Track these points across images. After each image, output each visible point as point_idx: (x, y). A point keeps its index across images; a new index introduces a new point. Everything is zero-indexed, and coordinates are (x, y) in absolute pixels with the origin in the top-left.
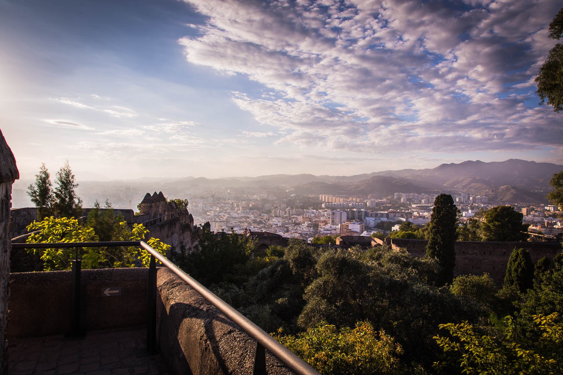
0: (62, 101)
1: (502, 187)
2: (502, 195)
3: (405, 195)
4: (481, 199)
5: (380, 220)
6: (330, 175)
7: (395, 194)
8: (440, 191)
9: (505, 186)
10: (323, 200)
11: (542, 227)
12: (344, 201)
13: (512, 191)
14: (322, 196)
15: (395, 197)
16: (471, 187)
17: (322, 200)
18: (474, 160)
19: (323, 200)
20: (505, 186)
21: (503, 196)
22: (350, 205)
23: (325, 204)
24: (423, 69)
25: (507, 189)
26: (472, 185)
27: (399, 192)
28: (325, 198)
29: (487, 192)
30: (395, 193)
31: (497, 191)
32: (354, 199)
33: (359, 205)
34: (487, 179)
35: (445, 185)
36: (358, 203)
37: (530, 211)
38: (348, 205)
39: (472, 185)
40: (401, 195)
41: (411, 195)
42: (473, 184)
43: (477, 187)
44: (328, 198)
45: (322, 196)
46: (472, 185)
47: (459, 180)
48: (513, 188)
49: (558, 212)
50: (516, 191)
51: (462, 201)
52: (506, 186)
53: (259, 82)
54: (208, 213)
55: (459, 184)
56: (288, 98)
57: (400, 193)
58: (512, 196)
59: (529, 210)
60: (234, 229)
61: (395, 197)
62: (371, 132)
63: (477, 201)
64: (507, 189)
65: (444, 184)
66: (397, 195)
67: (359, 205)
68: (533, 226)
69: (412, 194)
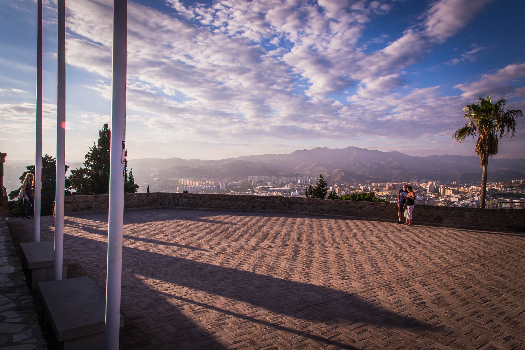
0: (93, 88)
6: (201, 159)
10: (182, 184)
12: (199, 184)
13: (342, 174)
14: (181, 180)
16: (316, 170)
17: (181, 183)
18: (322, 147)
19: (182, 184)
22: (203, 187)
23: (179, 188)
24: (190, 14)
27: (252, 175)
28: (181, 181)
32: (210, 182)
33: (211, 187)
36: (213, 185)
37: (341, 191)
38: (202, 188)
40: (255, 178)
44: (186, 181)
45: (181, 180)
54: (350, 186)
57: (254, 176)
58: (341, 177)
59: (340, 190)
61: (249, 180)
62: (384, 136)
64: (339, 172)
67: (211, 187)
69: (264, 177)
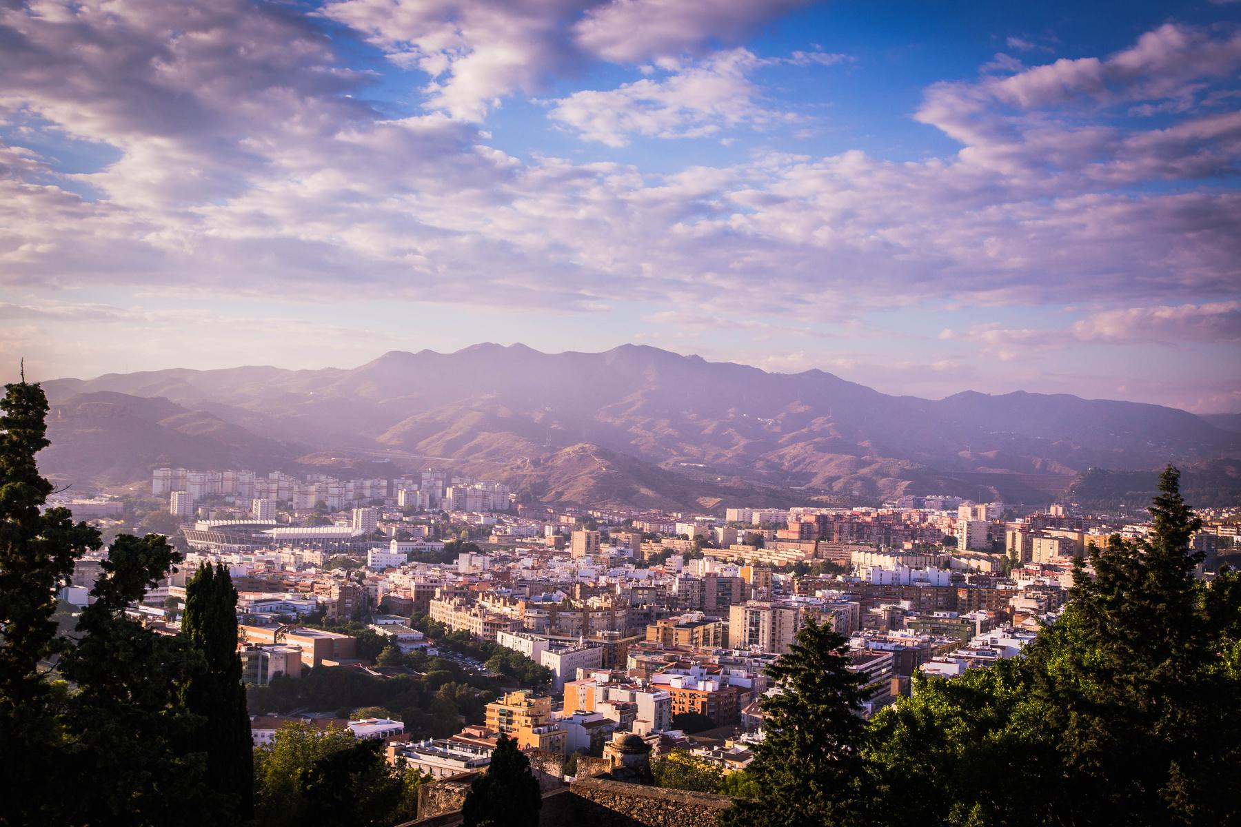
1: (567, 450)
2: (565, 479)
3: (198, 479)
4: (485, 495)
5: (512, 610)
7: (156, 473)
8: (347, 460)
9: (577, 447)
11: (527, 607)
13: (596, 466)
15: (157, 487)
16: (477, 448)
18: (506, 343)
20: (577, 447)
21: (567, 482)
25: (581, 458)
26: (478, 440)
27: (174, 466)
29: (519, 468)
30: (158, 468)
31: (550, 463)
34: (538, 417)
35: (383, 438)
37: (597, 543)
39: (482, 437)
40: (184, 477)
41: (228, 479)
42: (486, 434)
43: (495, 446)
46: (478, 440)
47: (438, 419)
48: (602, 453)
49: (682, 542)
50: (608, 463)
51: (419, 503)
52: (581, 445)
53: (1151, 30)
55: (435, 436)
56: (834, 55)
57: (181, 472)
59: (593, 539)
60: (434, 770)
61: (157, 487)
63: (470, 503)
64: (583, 458)
65: (384, 432)
66: (164, 478)
68: (505, 605)
69: (229, 474)
